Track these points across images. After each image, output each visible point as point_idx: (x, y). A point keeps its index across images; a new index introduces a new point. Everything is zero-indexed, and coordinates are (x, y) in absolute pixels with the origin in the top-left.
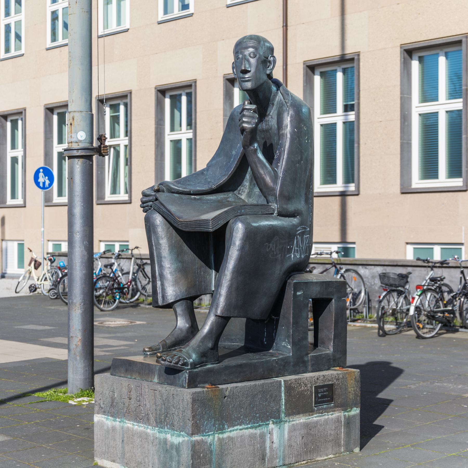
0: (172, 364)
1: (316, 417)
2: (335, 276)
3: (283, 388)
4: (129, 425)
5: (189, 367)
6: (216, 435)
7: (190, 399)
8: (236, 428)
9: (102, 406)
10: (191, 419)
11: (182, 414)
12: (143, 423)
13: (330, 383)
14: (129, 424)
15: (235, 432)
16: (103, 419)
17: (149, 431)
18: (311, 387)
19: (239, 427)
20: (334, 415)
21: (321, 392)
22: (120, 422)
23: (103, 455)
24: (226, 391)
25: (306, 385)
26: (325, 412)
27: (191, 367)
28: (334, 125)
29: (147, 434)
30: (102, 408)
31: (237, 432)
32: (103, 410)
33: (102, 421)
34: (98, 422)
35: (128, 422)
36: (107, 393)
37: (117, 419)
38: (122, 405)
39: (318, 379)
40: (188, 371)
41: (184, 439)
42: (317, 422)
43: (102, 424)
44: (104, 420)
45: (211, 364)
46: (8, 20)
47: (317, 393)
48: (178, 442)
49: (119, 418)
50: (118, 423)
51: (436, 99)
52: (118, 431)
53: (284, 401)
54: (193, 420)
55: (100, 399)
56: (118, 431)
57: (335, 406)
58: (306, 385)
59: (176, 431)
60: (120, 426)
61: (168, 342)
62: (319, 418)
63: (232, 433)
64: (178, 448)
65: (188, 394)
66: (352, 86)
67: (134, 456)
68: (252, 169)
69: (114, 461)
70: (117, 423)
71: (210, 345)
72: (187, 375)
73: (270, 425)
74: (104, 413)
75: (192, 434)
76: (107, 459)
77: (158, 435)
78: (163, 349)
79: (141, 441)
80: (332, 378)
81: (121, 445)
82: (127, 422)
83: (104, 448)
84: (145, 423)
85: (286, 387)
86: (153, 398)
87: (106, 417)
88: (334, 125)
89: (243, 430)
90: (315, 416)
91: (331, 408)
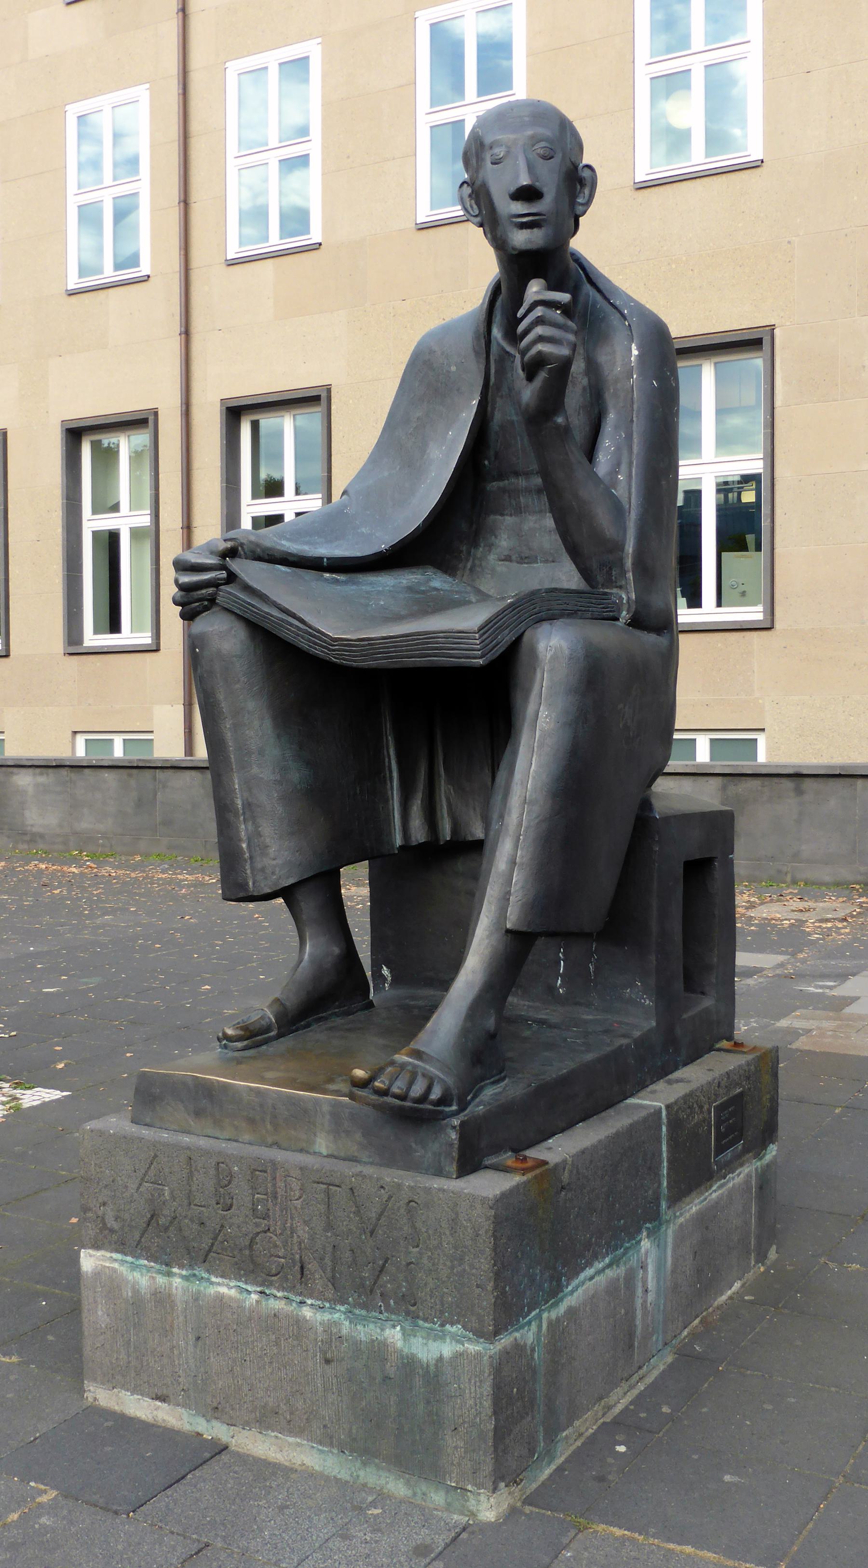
0: (408, 1104)
1: (715, 1191)
4: (223, 1290)
6: (545, 1315)
7: (488, 1219)
8: (582, 1276)
9: (111, 1223)
10: (490, 1286)
11: (452, 1268)
12: (281, 1288)
14: (225, 1288)
15: (580, 1290)
16: (116, 1265)
17: (307, 1313)
19: (589, 1272)
22: (186, 1278)
23: (118, 1377)
24: (564, 1169)
27: (459, 1105)
28: (97, 509)
29: (299, 1322)
30: (112, 1231)
31: (584, 1287)
32: (115, 1237)
33: (114, 1270)
34: (97, 1274)
35: (219, 1280)
36: (133, 1186)
37: (175, 1270)
38: (195, 1226)
41: (459, 1348)
43: (110, 1284)
44: (123, 1270)
45: (493, 1083)
48: (436, 1355)
49: (181, 1267)
50: (177, 1281)
51: (115, 508)
52: (180, 1307)
53: (665, 1164)
54: (496, 1288)
55: (104, 1204)
56: (180, 1307)
57: (746, 1150)
59: (425, 1320)
60: (185, 1290)
61: (292, 1002)
63: (575, 1294)
64: (434, 1378)
65: (479, 1206)
67: (246, 1388)
69: (162, 1398)
70: (177, 1282)
72: (454, 1136)
73: (642, 1243)
74: (121, 1246)
75: (496, 1333)
76: (135, 1390)
77: (346, 1327)
78: (279, 1028)
79: (277, 1343)
81: (191, 1349)
82: (214, 1279)
83: (123, 1356)
84: (292, 1289)
86: (322, 1208)
87: (129, 1259)
88: (97, 509)
89: (597, 1278)
90: (714, 1188)
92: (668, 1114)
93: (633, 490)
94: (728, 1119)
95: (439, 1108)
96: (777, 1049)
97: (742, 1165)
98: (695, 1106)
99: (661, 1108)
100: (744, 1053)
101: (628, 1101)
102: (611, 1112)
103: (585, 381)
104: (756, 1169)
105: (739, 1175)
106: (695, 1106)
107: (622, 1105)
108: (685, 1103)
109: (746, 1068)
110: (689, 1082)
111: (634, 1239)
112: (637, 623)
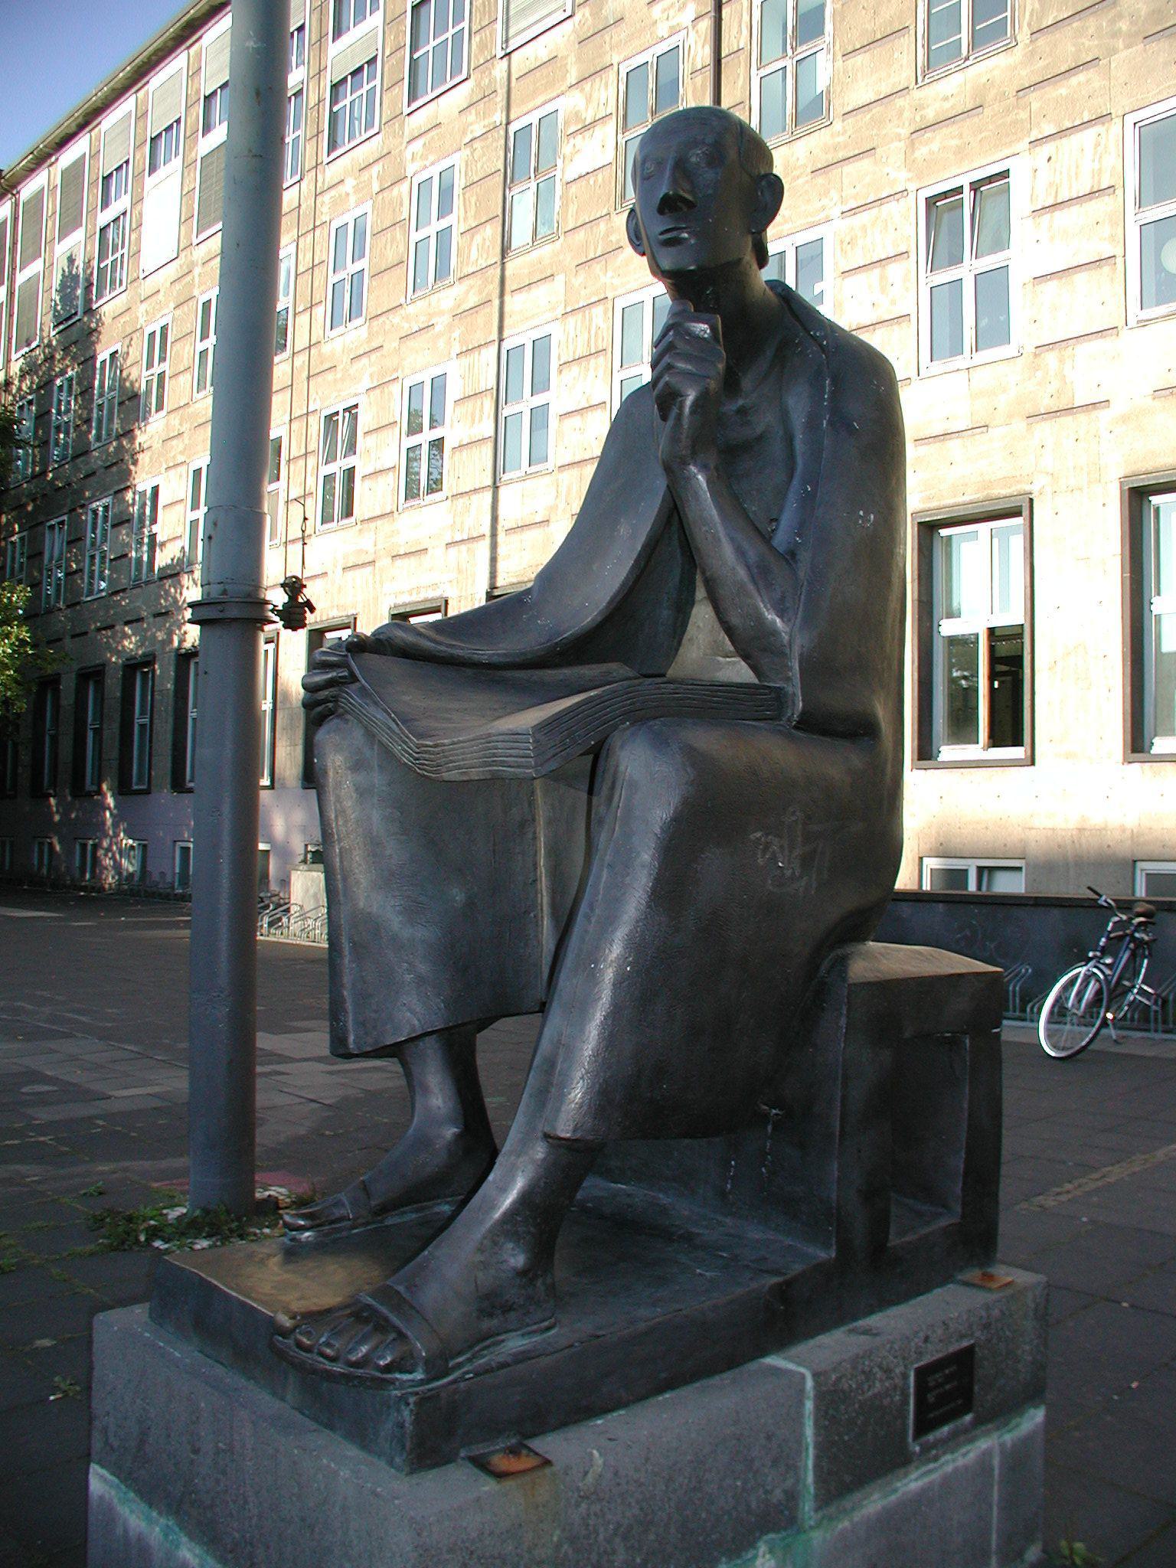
1: (916, 1480)
2: (188, 614)
3: (809, 1405)
5: (419, 1375)
13: (965, 1343)
18: (905, 1376)
20: (972, 1455)
21: (938, 1385)
25: (888, 1371)
26: (944, 1453)
27: (426, 1371)
39: (926, 1339)
40: (412, 1400)
42: (923, 1492)
46: (350, 461)
47: (922, 1389)
53: (811, 1451)
57: (978, 1422)
58: (888, 1371)
62: (926, 1480)
66: (479, 1257)
68: (703, 573)
71: (518, 1259)
80: (970, 1326)
85: (820, 1397)
90: (913, 1476)
91: (966, 1431)
92: (817, 1385)
93: (1152, 709)
94: (941, 1385)
95: (389, 1376)
96: (411, 1472)
97: (972, 1441)
98: (876, 1370)
99: (803, 1377)
100: (990, 1290)
101: (772, 1360)
102: (728, 1376)
103: (781, 433)
104: (1002, 1445)
105: (964, 1455)
106: (876, 1370)
107: (752, 1366)
108: (854, 1368)
109: (983, 1313)
110: (876, 1335)
111: (739, 1556)
112: (817, 725)
